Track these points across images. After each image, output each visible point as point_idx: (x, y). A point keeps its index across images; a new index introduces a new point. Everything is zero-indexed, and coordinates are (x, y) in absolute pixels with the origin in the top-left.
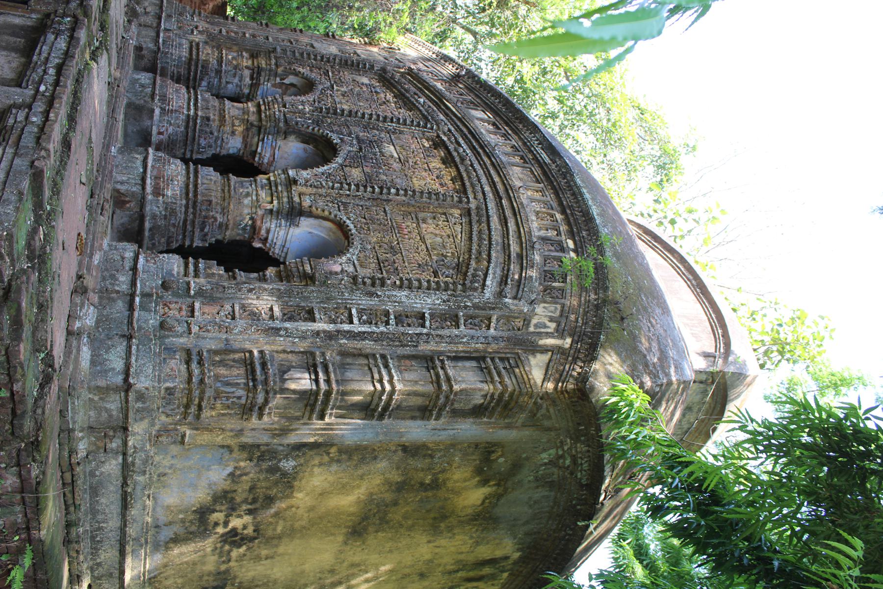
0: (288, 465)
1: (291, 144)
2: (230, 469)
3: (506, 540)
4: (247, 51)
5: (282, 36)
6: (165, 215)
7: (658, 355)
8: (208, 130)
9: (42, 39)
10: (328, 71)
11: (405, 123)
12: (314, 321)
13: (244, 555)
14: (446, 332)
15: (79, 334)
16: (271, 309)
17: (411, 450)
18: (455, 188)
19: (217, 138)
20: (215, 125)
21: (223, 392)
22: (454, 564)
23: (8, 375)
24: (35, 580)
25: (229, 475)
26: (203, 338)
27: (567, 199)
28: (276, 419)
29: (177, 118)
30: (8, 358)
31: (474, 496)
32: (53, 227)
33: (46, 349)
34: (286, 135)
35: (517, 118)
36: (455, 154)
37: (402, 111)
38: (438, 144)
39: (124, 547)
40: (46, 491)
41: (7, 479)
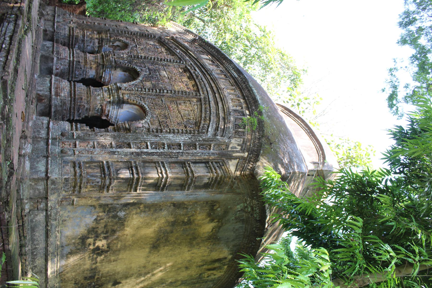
0: (121, 214)
2: (95, 217)
3: (224, 249)
4: (96, 31)
5: (112, 24)
6: (61, 105)
8: (79, 67)
10: (134, 39)
12: (131, 148)
13: (103, 260)
14: (191, 151)
15: (24, 156)
16: (111, 144)
17: (177, 205)
18: (194, 90)
19: (84, 71)
20: (82, 64)
21: (91, 180)
22: (201, 262)
24: (7, 270)
25: (95, 220)
27: (246, 93)
28: (115, 192)
29: (65, 62)
31: (208, 228)
32: (12, 106)
33: (11, 160)
34: (116, 68)
35: (222, 58)
36: (194, 74)
37: (169, 56)
38: (186, 70)
39: (47, 257)
40: (12, 225)
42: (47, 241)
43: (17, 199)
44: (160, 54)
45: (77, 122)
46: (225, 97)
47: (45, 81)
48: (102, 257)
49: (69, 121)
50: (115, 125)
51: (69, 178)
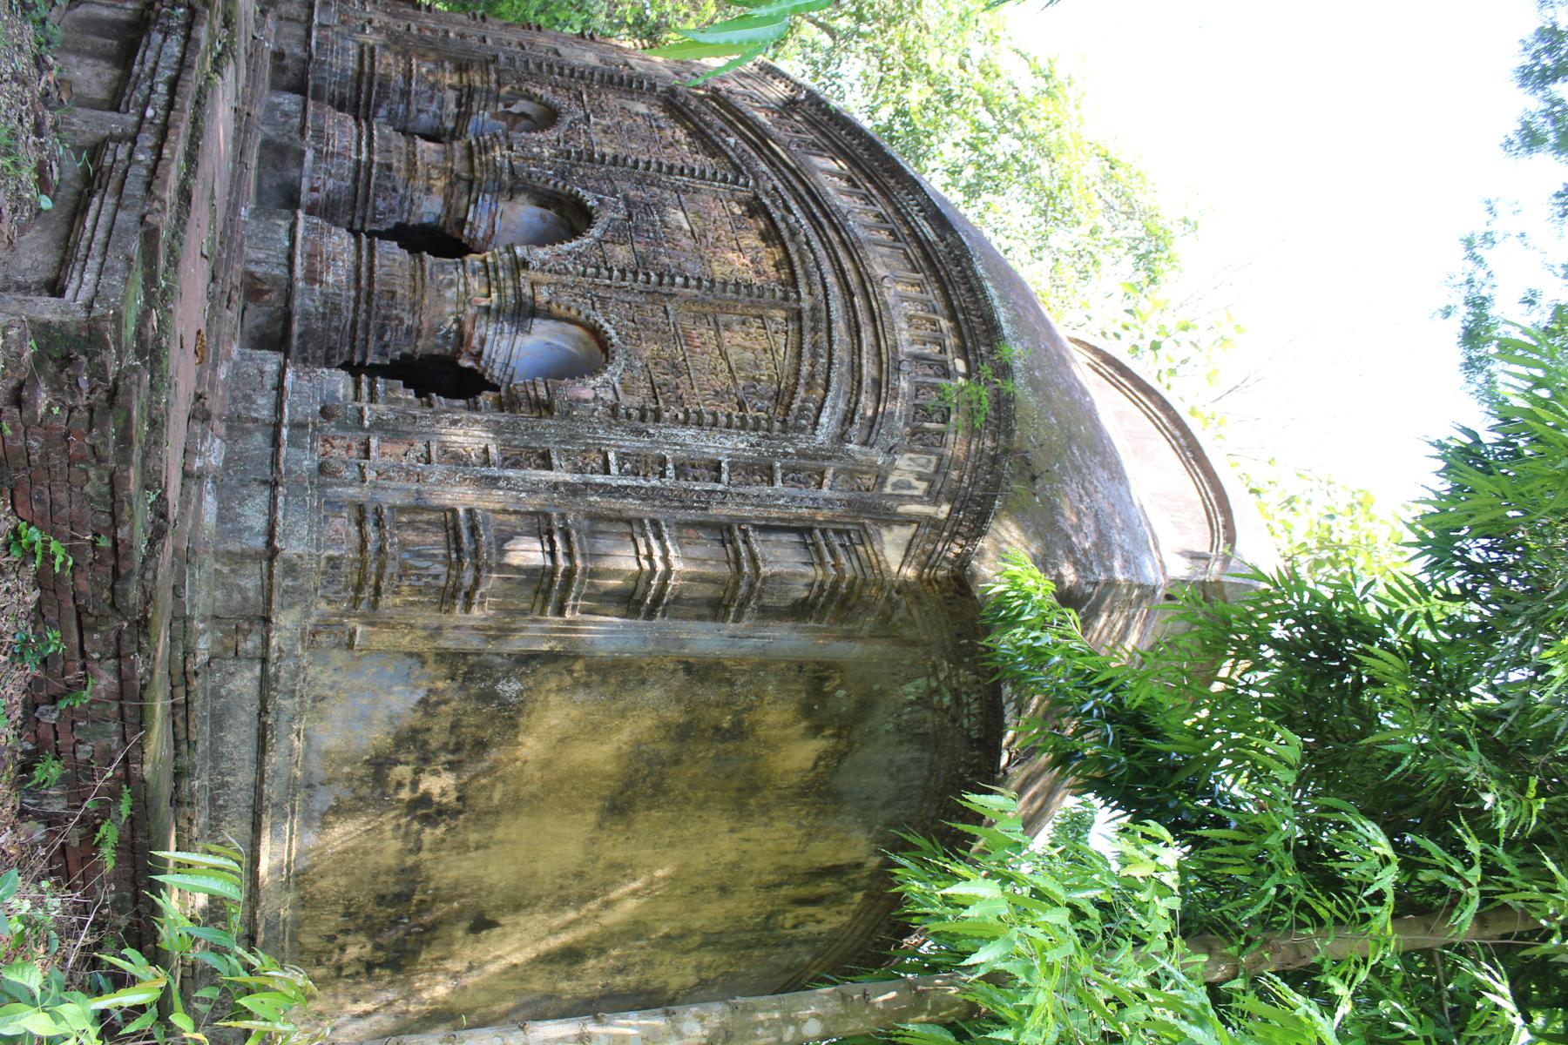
1: (520, 208)
2: (421, 693)
3: (855, 834)
4: (450, 59)
6: (324, 314)
7: (1093, 538)
8: (389, 185)
9: (144, 40)
11: (703, 176)
12: (550, 467)
13: (443, 840)
14: (754, 490)
15: (200, 477)
16: (486, 451)
17: (699, 670)
19: (404, 198)
22: (776, 871)
23: (112, 514)
24: (133, 846)
25: (420, 702)
26: (383, 488)
27: (960, 297)
29: (341, 166)
30: (113, 488)
31: (800, 754)
32: (170, 311)
34: (512, 193)
35: (886, 170)
36: (782, 226)
37: (700, 157)
38: (755, 208)
41: (100, 677)
42: (260, 763)
43: (174, 618)
44: (669, 151)
45: (374, 371)
46: (887, 308)
47: (273, 229)
48: (440, 831)
49: (347, 366)
50: (503, 390)
51: (341, 557)
